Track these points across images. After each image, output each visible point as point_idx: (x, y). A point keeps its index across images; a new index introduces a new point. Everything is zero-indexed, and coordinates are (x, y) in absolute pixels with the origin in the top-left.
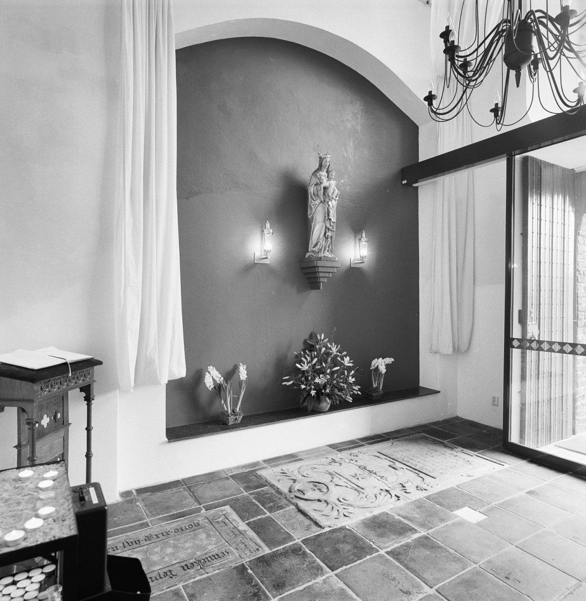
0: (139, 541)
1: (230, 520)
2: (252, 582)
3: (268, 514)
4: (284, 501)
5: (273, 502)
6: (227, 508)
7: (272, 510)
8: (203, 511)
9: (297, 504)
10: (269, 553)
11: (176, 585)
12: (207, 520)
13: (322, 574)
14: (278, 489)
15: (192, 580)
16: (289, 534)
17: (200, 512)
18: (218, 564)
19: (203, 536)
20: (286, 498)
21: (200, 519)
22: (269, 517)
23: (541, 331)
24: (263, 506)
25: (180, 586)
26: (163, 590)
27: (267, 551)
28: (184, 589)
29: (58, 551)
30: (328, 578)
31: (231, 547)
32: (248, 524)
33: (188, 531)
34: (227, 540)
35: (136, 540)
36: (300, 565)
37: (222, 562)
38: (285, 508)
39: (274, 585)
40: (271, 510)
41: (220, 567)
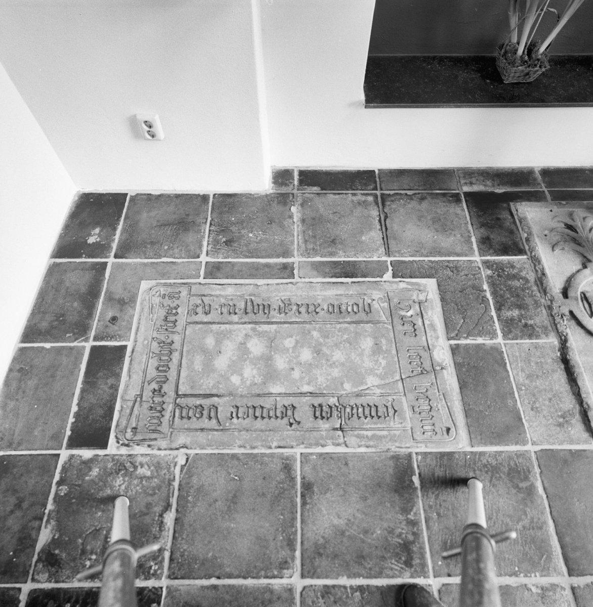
0: (269, 306)
1: (427, 322)
2: (411, 510)
3: (500, 340)
4: (541, 318)
5: (520, 307)
6: (431, 284)
7: (511, 332)
8: (388, 276)
9: (566, 341)
10: (465, 454)
11: (292, 447)
12: (386, 305)
13: (546, 571)
14: (544, 274)
15: (319, 450)
16: (520, 419)
17: (382, 277)
18: (369, 433)
19: (367, 344)
20: (550, 308)
21: (377, 295)
22: (496, 350)
23: (542, 469)
24: (498, 310)
25: (298, 451)
26: (270, 448)
27: (461, 443)
28: (301, 462)
29: (96, 224)
30: (554, 587)
31: (404, 399)
32: (454, 350)
33: (348, 320)
34: (403, 377)
35: (265, 303)
36: (510, 516)
37: (378, 433)
38: (538, 337)
39: (560, 425)
40: (509, 327)
41: (371, 443)
